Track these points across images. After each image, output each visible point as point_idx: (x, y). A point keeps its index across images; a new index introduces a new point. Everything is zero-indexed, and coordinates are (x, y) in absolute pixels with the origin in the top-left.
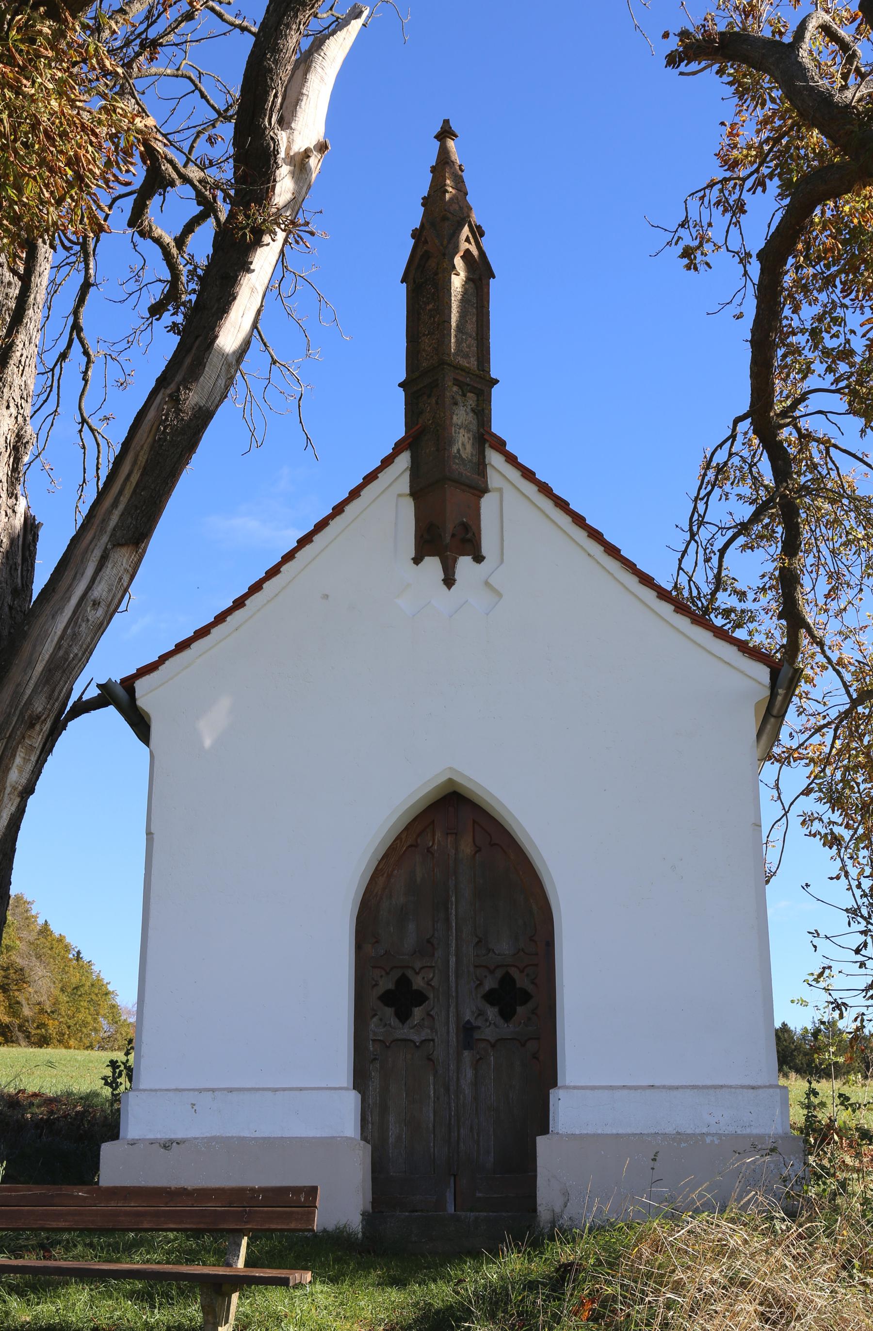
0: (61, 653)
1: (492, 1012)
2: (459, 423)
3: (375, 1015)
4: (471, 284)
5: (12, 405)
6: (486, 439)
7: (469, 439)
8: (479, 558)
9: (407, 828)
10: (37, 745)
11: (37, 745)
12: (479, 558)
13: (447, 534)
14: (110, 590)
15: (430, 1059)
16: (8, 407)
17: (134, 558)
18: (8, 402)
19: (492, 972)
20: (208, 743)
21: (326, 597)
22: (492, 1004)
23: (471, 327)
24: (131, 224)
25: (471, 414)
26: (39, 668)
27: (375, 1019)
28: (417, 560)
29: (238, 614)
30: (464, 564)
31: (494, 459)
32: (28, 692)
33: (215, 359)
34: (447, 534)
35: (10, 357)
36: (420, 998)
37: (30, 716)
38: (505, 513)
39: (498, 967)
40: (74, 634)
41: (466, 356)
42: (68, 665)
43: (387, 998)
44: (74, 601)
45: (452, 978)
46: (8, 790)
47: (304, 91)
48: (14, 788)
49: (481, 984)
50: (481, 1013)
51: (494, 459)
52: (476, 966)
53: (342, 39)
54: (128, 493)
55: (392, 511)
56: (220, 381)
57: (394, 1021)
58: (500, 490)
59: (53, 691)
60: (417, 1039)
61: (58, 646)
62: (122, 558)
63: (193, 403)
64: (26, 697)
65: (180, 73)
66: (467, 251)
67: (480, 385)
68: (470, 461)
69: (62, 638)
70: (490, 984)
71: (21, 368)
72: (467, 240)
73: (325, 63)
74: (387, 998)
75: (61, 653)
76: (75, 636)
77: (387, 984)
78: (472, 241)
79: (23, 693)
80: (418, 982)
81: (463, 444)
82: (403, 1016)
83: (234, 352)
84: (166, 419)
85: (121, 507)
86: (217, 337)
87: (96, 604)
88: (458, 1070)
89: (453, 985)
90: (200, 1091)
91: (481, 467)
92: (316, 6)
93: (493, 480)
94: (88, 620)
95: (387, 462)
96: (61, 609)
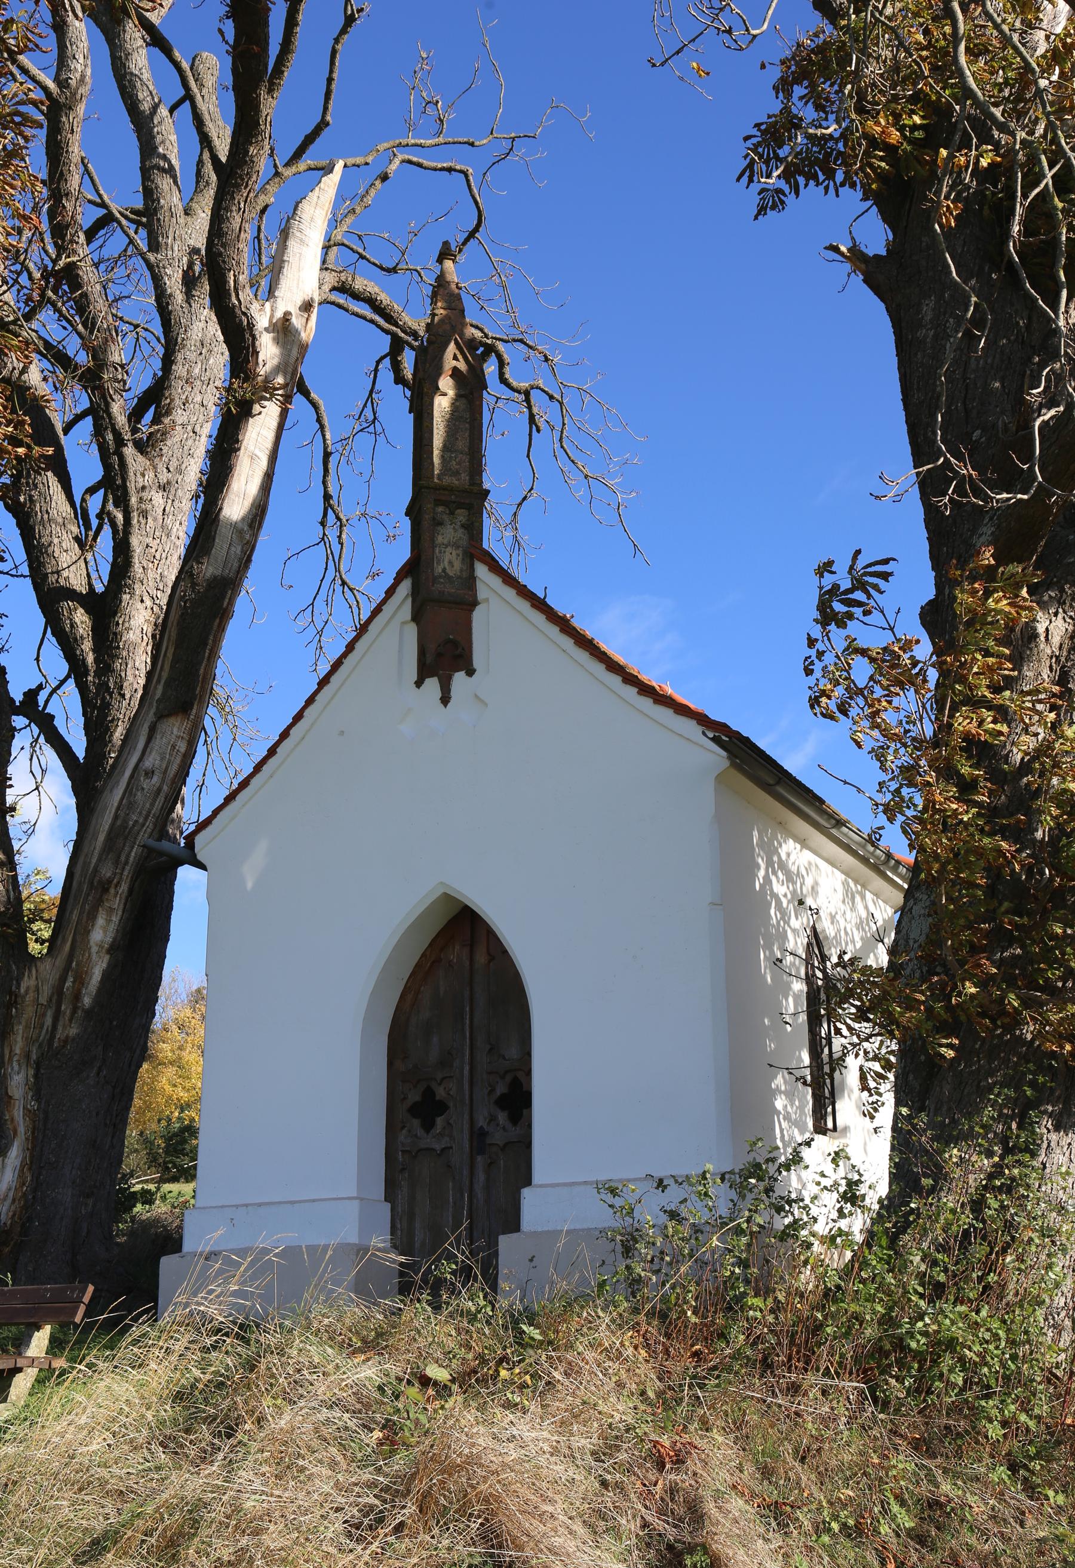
0: (119, 823)
1: (502, 1117)
2: (445, 542)
3: (403, 1128)
4: (464, 401)
5: (146, 598)
6: (475, 552)
7: (458, 555)
8: (471, 672)
9: (431, 945)
10: (116, 906)
11: (116, 906)
12: (471, 672)
13: (445, 656)
14: (162, 759)
15: (449, 1166)
16: (142, 601)
17: (187, 725)
18: (141, 596)
19: (503, 1077)
20: (250, 885)
21: (342, 733)
22: (503, 1109)
23: (462, 444)
24: (397, 382)
25: (461, 530)
26: (102, 837)
27: (404, 1131)
28: (419, 684)
29: (272, 761)
30: (459, 677)
31: (481, 571)
32: (94, 861)
33: (223, 530)
34: (445, 656)
35: (132, 557)
36: (441, 1108)
37: (100, 882)
38: (497, 624)
39: (506, 1072)
40: (130, 803)
41: (456, 473)
42: (130, 832)
43: (414, 1110)
44: (128, 773)
45: (466, 1086)
46: (94, 949)
47: (285, 258)
48: (101, 947)
49: (492, 1091)
50: (492, 1119)
51: (481, 571)
52: (490, 1073)
53: (315, 199)
54: (167, 667)
55: (398, 640)
56: (233, 549)
57: (420, 1132)
58: (487, 600)
59: (119, 857)
60: (438, 1147)
61: (116, 817)
62: (174, 729)
63: (208, 575)
64: (92, 865)
65: (332, 242)
66: (455, 369)
67: (472, 499)
68: (460, 577)
69: (118, 808)
70: (501, 1089)
71: (156, 562)
72: (455, 358)
73: (302, 226)
74: (414, 1110)
75: (119, 823)
76: (131, 806)
77: (414, 1096)
78: (460, 357)
79: (90, 863)
80: (440, 1093)
81: (450, 562)
82: (428, 1126)
83: (243, 519)
84: (185, 595)
85: (163, 682)
86: (221, 509)
87: (149, 774)
88: (472, 1174)
89: (467, 1093)
90: (237, 1206)
91: (470, 581)
92: (250, 183)
93: (482, 593)
94: (143, 789)
95: (390, 592)
96: (118, 782)
